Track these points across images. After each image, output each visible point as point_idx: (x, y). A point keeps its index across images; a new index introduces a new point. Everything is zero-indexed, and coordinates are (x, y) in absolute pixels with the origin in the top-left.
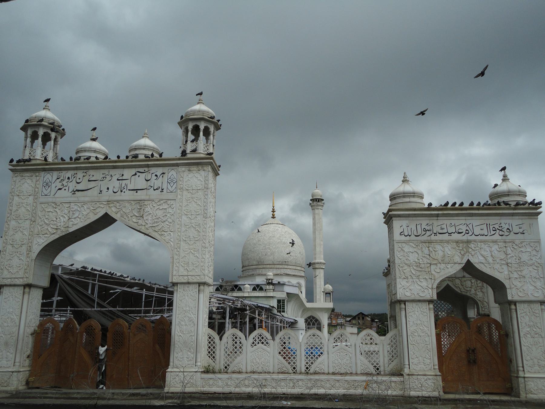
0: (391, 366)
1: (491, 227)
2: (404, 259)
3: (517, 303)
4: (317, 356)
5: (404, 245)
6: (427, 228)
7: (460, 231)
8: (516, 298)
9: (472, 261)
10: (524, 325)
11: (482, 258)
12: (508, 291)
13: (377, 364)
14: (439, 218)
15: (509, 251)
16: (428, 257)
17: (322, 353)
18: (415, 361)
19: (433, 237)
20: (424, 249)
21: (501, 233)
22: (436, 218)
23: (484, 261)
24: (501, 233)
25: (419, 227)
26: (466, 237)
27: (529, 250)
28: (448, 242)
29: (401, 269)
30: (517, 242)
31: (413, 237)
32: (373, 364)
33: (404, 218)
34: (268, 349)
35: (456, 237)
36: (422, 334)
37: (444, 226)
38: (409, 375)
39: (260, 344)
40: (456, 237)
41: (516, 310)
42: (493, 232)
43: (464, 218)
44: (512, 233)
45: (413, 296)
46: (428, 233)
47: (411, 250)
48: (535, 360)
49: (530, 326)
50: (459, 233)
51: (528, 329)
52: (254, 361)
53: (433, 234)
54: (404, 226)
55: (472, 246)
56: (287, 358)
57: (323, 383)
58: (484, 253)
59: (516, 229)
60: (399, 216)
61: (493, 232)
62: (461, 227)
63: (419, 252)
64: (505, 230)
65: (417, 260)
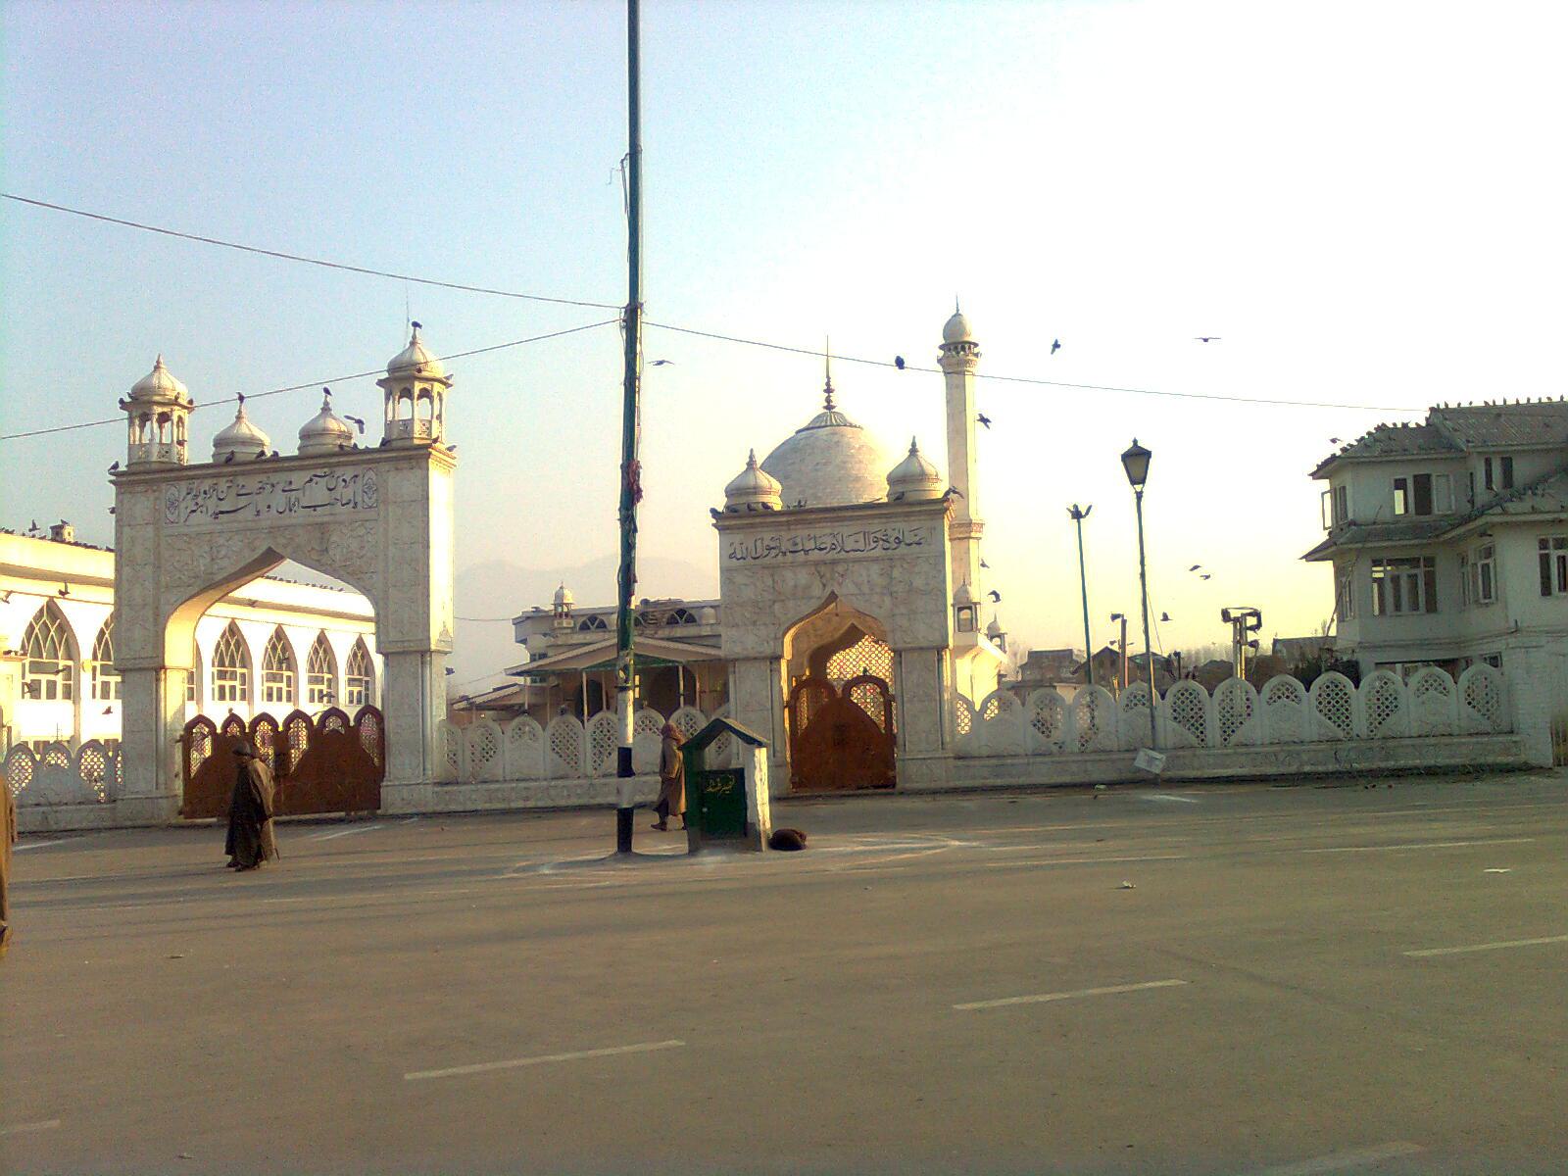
14: (792, 527)
21: (887, 545)
24: (887, 545)
25: (759, 543)
31: (749, 560)
46: (773, 552)
54: (736, 545)
55: (840, 569)
62: (824, 539)
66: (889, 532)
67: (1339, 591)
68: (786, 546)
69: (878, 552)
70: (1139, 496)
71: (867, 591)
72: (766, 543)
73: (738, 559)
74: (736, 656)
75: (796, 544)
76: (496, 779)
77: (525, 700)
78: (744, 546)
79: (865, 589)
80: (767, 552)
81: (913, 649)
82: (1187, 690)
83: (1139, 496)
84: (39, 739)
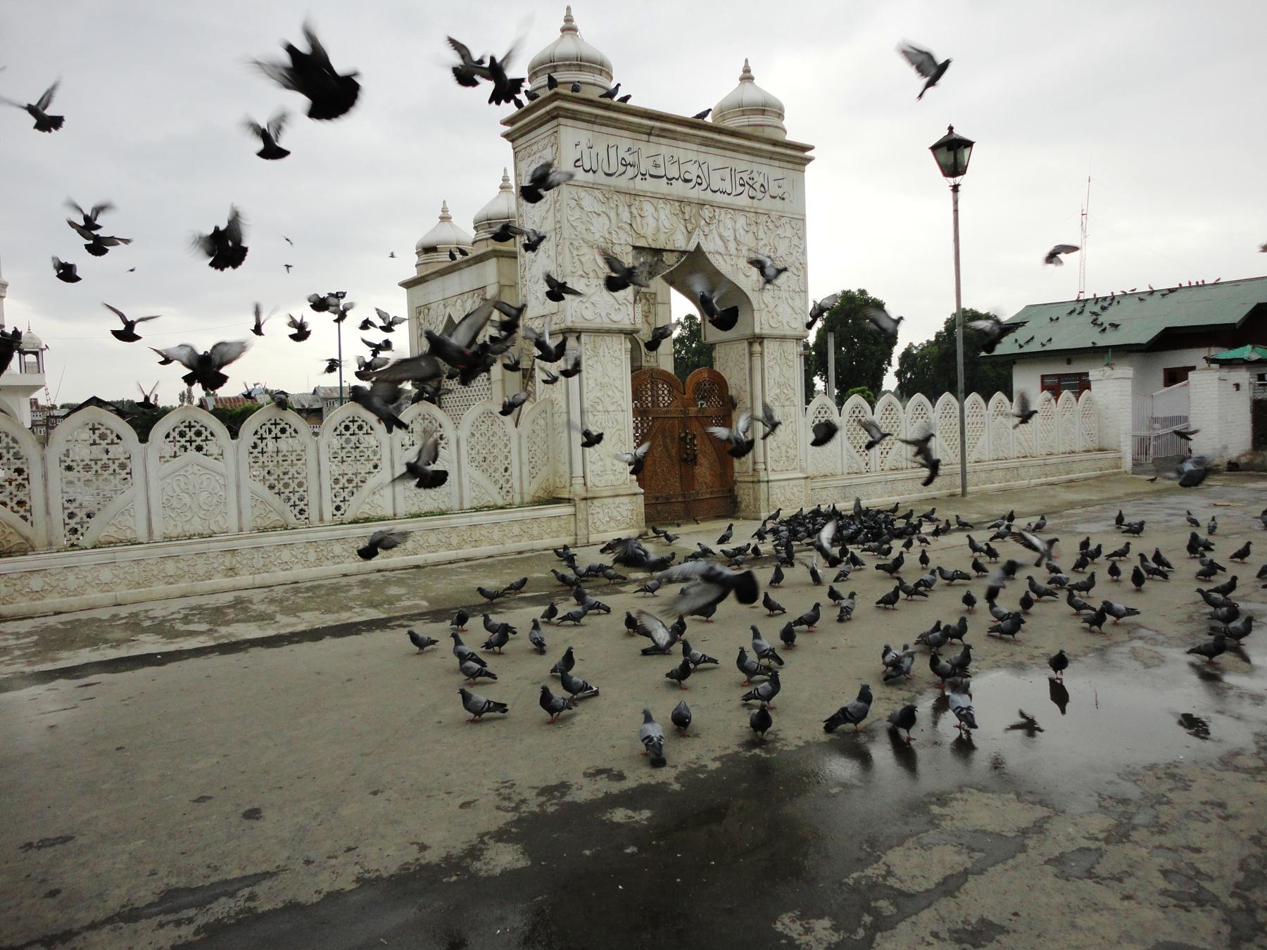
0: (534, 486)
1: (738, 176)
2: (581, 228)
3: (583, 337)
4: (272, 479)
5: (583, 194)
6: (629, 159)
7: (688, 176)
8: (766, 331)
9: (705, 248)
10: (772, 382)
11: (721, 244)
12: (756, 315)
13: (301, 499)
14: (652, 138)
15: (761, 235)
16: (628, 227)
17: (376, 467)
18: (597, 468)
19: (640, 184)
20: (621, 209)
21: (752, 193)
22: (645, 137)
23: (722, 250)
25: (612, 151)
26: (696, 193)
27: (788, 234)
28: (665, 199)
29: (575, 253)
30: (774, 215)
31: (600, 178)
32: (496, 482)
33: (584, 125)
34: (219, 465)
35: (679, 188)
36: (611, 408)
37: (660, 160)
38: (585, 499)
39: (192, 453)
40: (679, 188)
41: (762, 354)
42: (740, 189)
43: (746, 157)
44: (767, 195)
45: (598, 320)
46: (631, 172)
47: (598, 208)
48: (784, 448)
49: (602, 386)
50: (686, 181)
51: (599, 394)
52: (175, 503)
53: (640, 176)
54: (583, 146)
55: (706, 212)
56: (279, 486)
57: (484, 532)
58: (725, 234)
59: (774, 190)
60: (574, 116)
61: (740, 189)
62: (689, 167)
63: (613, 215)
64: (757, 186)
65: (607, 236)
66: (755, 175)
67: (126, 409)
68: (646, 166)
69: (743, 201)
70: (955, 188)
71: (733, 251)
72: (622, 154)
73: (587, 171)
74: (586, 325)
75: (656, 166)
76: (129, 535)
77: (646, 308)
78: (593, 152)
79: (732, 246)
80: (622, 169)
81: (775, 338)
82: (190, 427)
83: (955, 188)
84: (1191, 419)
